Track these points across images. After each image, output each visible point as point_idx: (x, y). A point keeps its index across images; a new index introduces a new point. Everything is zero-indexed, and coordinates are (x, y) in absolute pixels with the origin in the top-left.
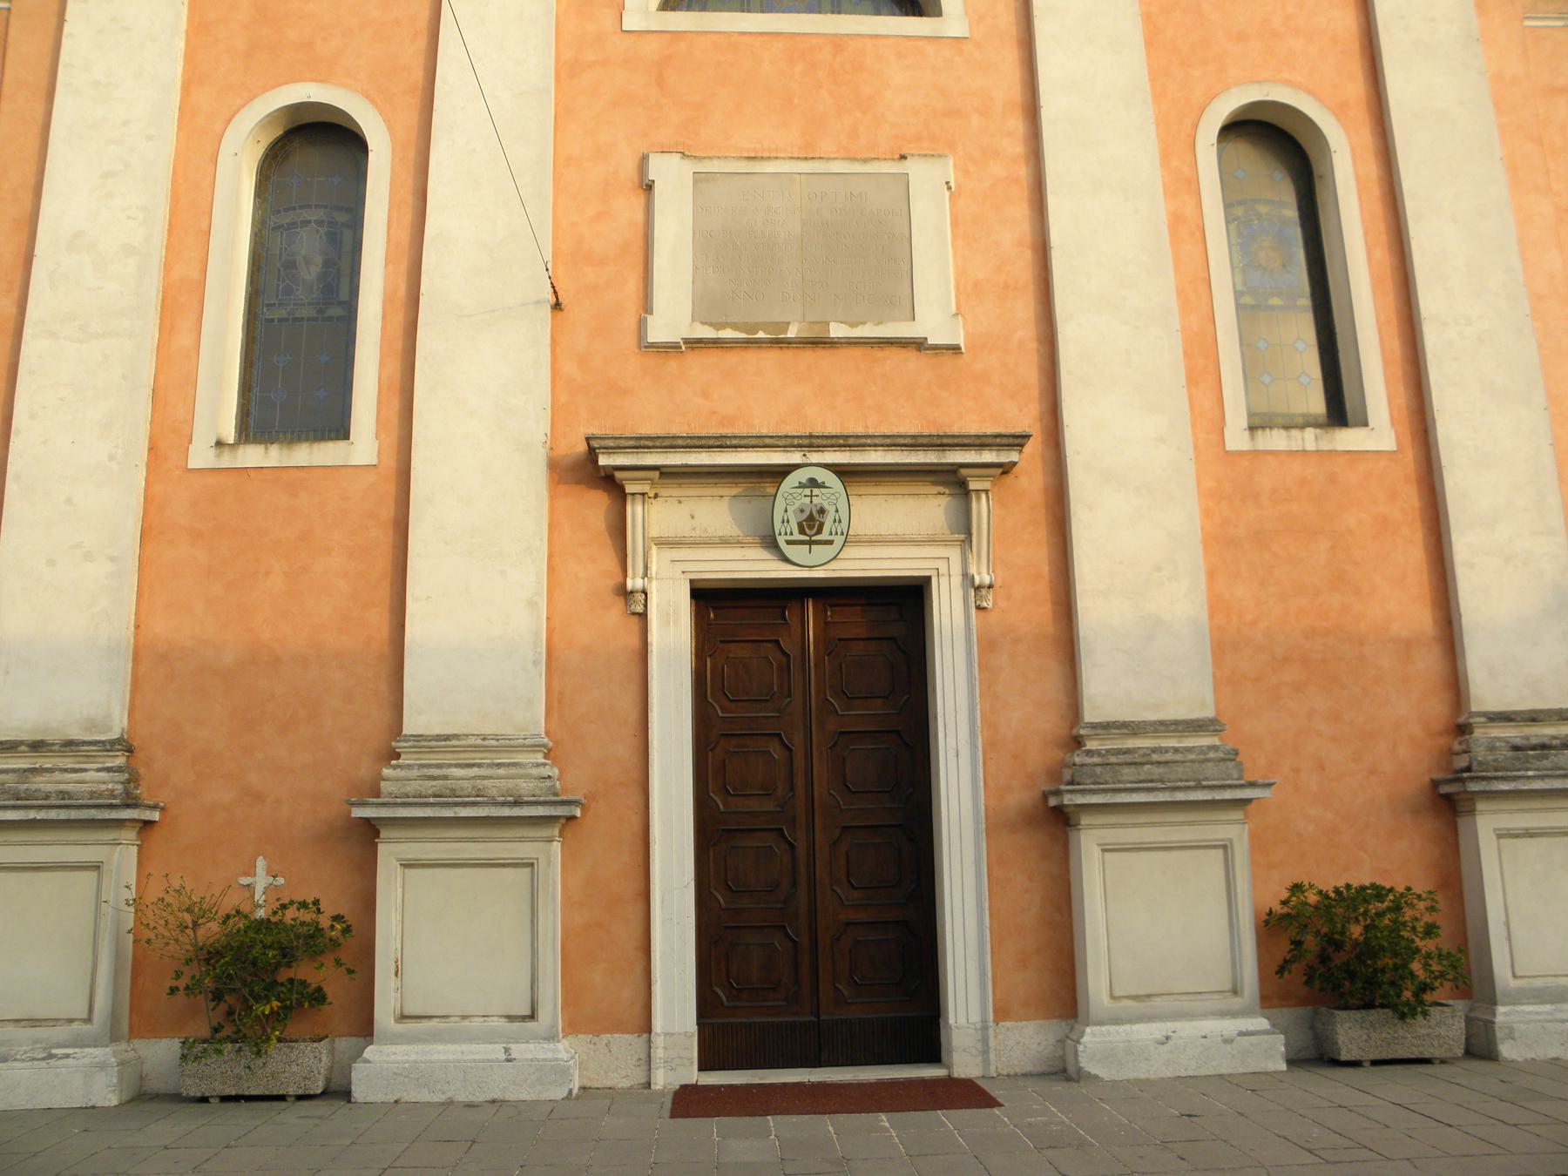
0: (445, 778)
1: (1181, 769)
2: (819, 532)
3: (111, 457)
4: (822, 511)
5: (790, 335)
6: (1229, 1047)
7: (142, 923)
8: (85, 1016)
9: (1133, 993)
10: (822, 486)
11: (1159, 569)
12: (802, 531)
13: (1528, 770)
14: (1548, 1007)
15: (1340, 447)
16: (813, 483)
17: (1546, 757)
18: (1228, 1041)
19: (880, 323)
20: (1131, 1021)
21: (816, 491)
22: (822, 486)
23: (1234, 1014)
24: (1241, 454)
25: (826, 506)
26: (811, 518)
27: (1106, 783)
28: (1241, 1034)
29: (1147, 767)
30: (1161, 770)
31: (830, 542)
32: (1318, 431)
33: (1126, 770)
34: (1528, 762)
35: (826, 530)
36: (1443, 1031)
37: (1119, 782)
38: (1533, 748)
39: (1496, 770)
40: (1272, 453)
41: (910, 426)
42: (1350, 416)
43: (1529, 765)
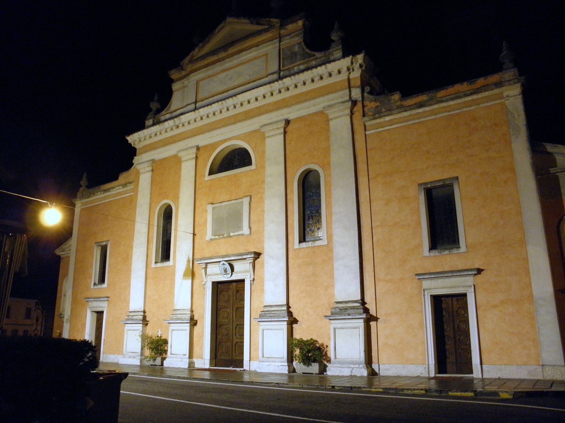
0: (177, 316)
1: (276, 314)
2: (227, 272)
3: (142, 267)
4: (226, 269)
5: (225, 236)
6: (278, 368)
7: (237, 338)
8: (172, 353)
9: (267, 357)
10: (225, 264)
11: (278, 275)
12: (225, 272)
13: (342, 314)
14: (340, 365)
15: (316, 245)
16: (223, 264)
17: (346, 311)
18: (278, 366)
19: (238, 231)
20: (265, 362)
21: (224, 265)
22: (225, 264)
23: (282, 362)
24: (297, 249)
25: (227, 268)
26: (225, 270)
27: (264, 317)
28: (281, 365)
29: (271, 314)
30: (273, 315)
31: (229, 274)
32: (312, 242)
33: (268, 315)
34: (342, 312)
35: (228, 272)
36: (314, 368)
37: (266, 317)
38: (344, 309)
39: (336, 314)
40: (303, 248)
41: (236, 252)
42: (301, 244)
43: (342, 313)
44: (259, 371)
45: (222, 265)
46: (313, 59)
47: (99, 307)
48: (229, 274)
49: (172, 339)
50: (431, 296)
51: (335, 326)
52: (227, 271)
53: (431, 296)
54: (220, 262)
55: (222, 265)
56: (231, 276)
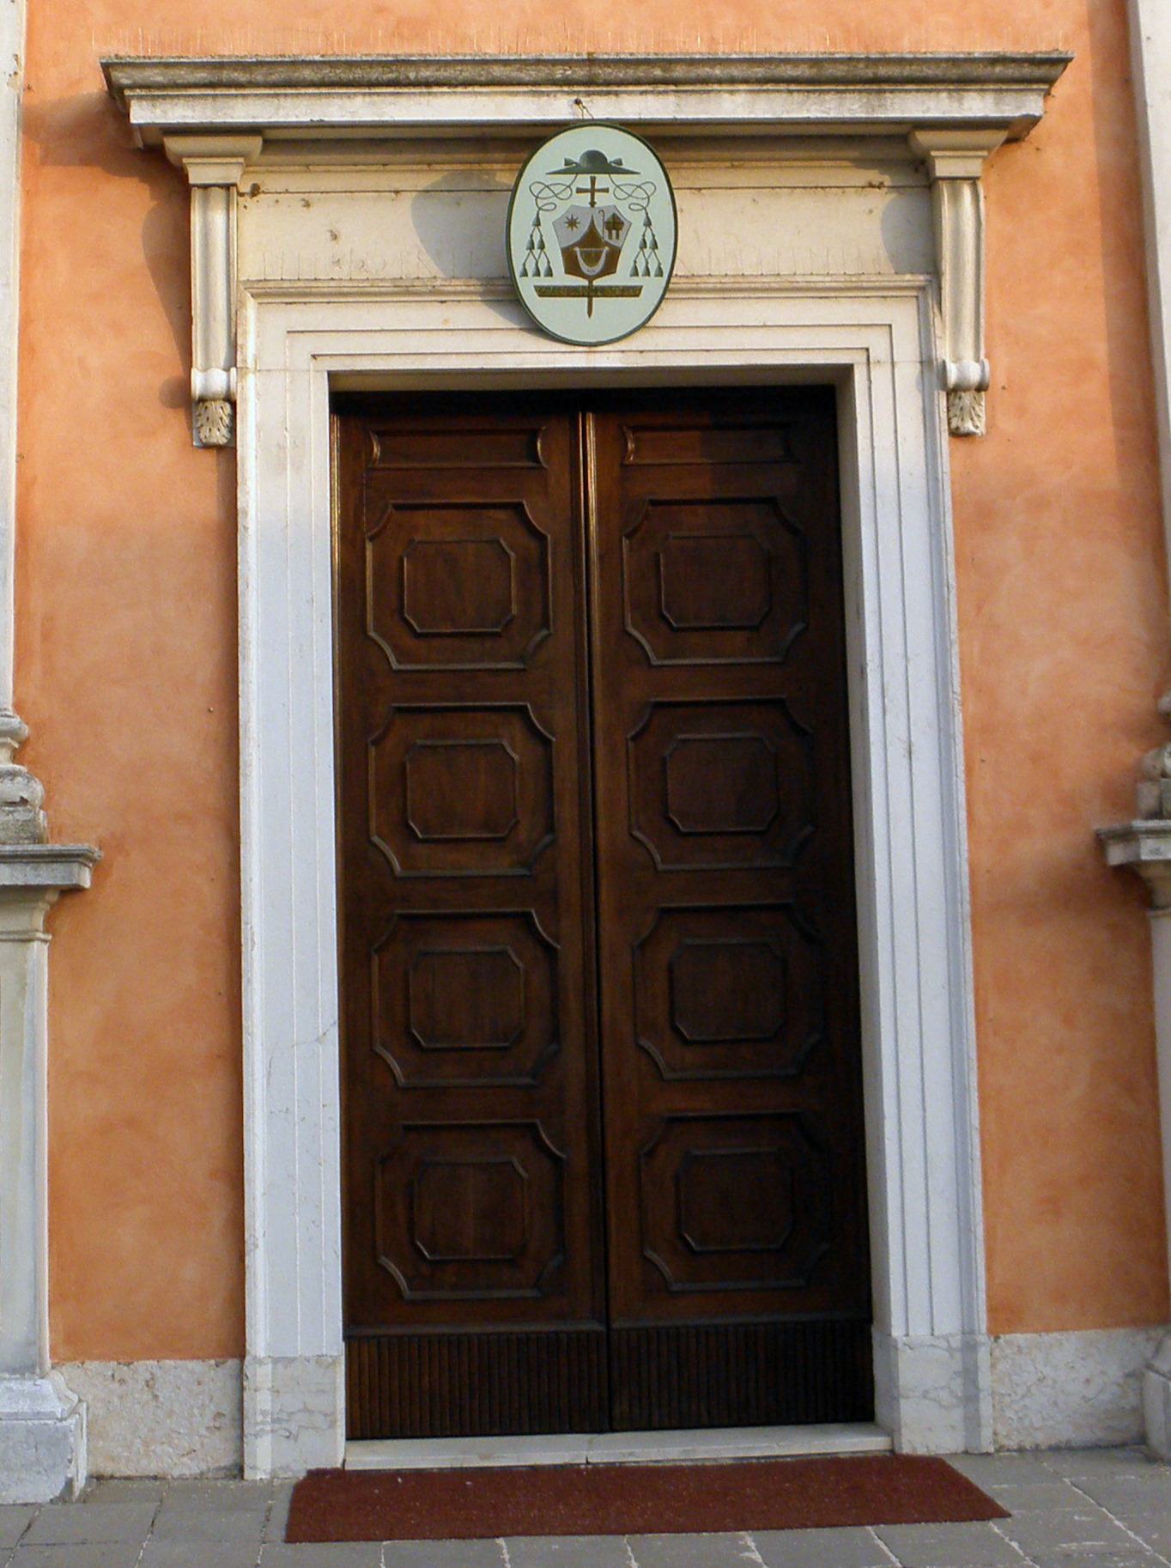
2: (610, 268)
4: (615, 224)
10: (615, 168)
12: (572, 267)
16: (596, 163)
21: (602, 180)
22: (615, 168)
26: (591, 239)
31: (634, 292)
35: (624, 264)
44: (638, 1536)
45: (571, 168)
46: (993, 90)
47: (490, 301)
48: (634, 292)
49: (471, 351)
50: (846, 371)
51: (127, 51)
52: (614, 255)
53: (846, 371)
54: (528, 138)
55: (571, 168)
56: (524, 264)
